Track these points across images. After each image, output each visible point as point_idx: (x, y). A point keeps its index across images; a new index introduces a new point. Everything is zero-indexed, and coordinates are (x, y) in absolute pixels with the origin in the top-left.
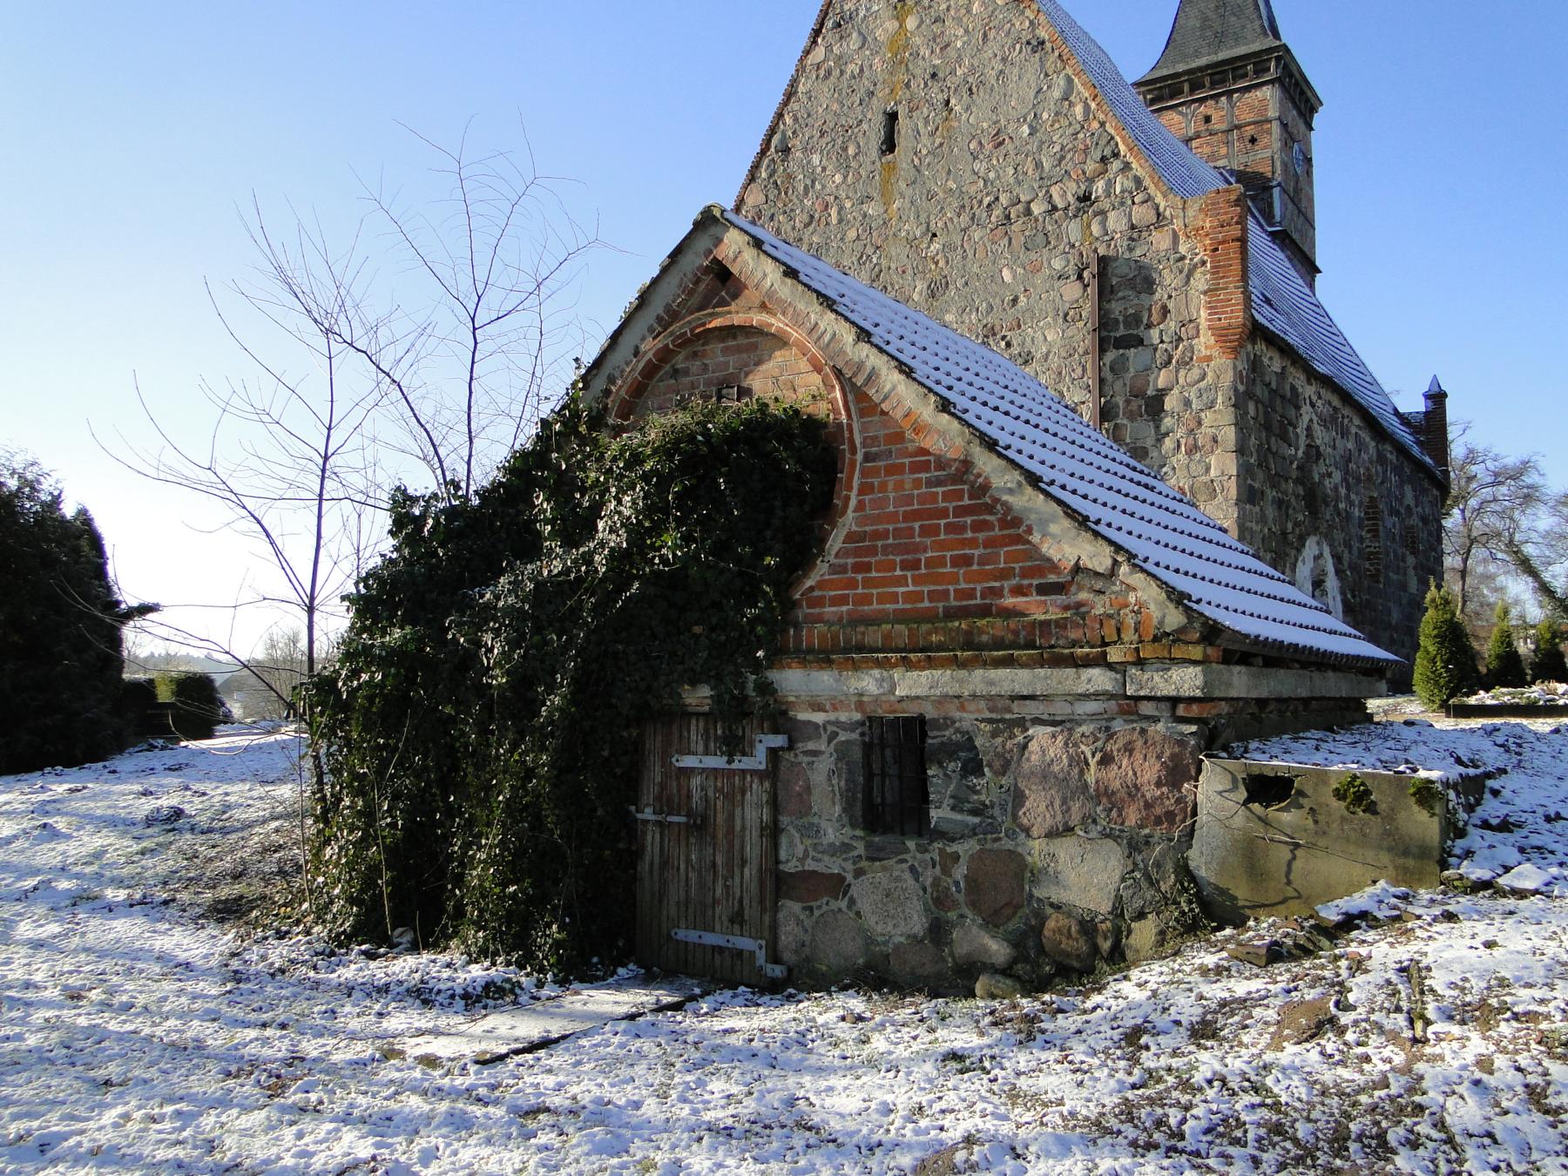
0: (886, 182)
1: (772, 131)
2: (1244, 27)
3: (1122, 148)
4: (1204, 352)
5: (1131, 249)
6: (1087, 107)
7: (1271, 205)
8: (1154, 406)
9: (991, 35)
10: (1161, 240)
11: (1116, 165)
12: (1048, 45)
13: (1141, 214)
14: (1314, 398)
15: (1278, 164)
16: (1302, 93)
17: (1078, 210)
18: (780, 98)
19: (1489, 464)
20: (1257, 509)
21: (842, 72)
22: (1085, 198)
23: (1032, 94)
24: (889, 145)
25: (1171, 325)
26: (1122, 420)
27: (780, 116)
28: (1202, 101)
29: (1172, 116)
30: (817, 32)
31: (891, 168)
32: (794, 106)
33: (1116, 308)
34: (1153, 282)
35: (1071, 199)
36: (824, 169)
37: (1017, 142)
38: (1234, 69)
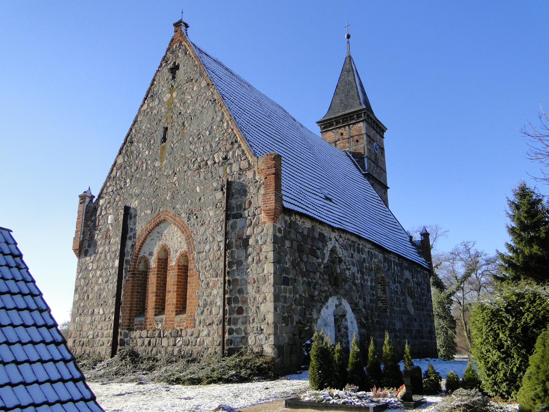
0: (162, 153)
1: (128, 135)
2: (354, 103)
3: (238, 138)
4: (263, 220)
5: (239, 178)
6: (228, 123)
7: (364, 164)
8: (245, 243)
9: (199, 98)
10: (250, 175)
11: (236, 145)
12: (217, 101)
13: (244, 164)
14: (338, 238)
15: (366, 149)
16: (377, 125)
17: (223, 163)
18: (132, 123)
19: (483, 257)
20: (291, 287)
21: (152, 113)
22: (226, 158)
23: (211, 119)
24: (164, 139)
25: (252, 208)
26: (234, 249)
27: (131, 130)
28: (340, 128)
29: (330, 133)
30: (145, 99)
31: (164, 148)
32: (136, 126)
33: (233, 202)
34: (246, 192)
35: (221, 159)
36: (143, 149)
37: (205, 137)
38: (350, 117)
